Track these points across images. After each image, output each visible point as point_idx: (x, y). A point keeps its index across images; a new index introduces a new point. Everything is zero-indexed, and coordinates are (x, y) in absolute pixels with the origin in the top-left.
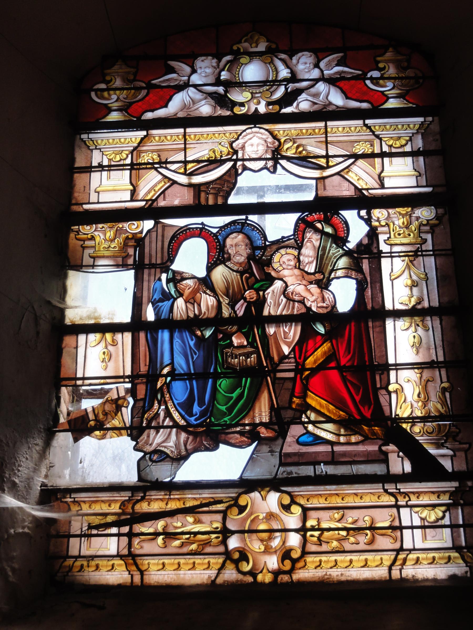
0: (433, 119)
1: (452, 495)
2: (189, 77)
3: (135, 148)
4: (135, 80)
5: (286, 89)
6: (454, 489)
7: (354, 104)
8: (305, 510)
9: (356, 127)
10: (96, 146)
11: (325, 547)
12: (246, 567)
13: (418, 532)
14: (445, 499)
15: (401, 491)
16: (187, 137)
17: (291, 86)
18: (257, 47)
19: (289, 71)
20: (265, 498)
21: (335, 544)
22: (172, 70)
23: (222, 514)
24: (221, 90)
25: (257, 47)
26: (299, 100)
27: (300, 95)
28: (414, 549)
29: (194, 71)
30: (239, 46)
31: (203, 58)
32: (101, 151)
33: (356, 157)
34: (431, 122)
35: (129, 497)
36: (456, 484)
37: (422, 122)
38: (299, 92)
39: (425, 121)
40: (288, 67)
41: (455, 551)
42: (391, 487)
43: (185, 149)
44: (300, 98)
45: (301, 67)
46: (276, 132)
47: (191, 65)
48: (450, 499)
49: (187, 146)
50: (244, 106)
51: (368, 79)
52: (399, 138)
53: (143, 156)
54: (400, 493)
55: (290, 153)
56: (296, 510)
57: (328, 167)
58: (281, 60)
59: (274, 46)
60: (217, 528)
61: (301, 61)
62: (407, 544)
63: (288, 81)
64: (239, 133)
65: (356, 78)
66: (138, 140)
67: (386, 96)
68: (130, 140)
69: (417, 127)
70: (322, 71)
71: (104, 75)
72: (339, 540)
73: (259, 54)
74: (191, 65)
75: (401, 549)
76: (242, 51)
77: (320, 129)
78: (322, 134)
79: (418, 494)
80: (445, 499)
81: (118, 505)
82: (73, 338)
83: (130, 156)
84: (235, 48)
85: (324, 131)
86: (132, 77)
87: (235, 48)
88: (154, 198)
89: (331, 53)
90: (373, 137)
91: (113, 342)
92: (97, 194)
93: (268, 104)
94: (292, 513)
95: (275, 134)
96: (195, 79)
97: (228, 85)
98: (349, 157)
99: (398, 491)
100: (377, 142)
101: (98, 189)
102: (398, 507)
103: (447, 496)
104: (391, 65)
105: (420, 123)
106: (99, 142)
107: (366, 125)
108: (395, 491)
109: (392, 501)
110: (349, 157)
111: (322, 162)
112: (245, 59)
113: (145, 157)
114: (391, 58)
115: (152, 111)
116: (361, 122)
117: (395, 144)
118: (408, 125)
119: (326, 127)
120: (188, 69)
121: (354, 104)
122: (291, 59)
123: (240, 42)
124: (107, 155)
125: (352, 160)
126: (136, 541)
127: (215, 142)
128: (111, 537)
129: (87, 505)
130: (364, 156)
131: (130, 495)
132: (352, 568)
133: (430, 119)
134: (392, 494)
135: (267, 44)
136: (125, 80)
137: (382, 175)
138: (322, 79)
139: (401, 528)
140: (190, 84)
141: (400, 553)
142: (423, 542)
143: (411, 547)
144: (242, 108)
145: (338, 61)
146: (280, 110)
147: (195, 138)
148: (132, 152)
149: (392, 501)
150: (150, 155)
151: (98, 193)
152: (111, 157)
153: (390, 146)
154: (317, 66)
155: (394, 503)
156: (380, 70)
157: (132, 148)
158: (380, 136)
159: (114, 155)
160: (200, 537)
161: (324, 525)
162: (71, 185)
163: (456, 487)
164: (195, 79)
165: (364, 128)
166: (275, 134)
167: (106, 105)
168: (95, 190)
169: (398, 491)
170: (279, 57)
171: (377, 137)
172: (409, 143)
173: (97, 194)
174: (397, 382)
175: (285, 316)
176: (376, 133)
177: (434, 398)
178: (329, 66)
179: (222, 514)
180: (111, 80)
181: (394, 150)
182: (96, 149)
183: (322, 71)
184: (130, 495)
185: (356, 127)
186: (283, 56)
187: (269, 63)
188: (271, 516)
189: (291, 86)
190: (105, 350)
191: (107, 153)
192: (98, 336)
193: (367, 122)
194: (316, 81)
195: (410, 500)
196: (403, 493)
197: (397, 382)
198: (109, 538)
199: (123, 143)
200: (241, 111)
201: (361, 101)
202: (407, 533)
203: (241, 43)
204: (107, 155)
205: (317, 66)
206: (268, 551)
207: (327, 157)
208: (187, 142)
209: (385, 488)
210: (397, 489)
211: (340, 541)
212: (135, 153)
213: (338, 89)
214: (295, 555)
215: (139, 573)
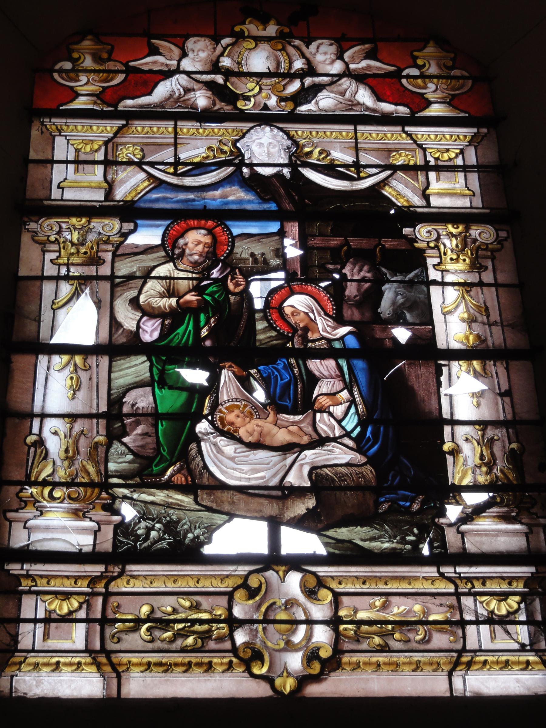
0: (488, 131)
1: (528, 581)
2: (179, 61)
3: (110, 140)
4: (109, 59)
5: (303, 84)
6: (530, 575)
7: (387, 107)
8: (337, 596)
9: (378, 134)
10: (60, 132)
11: (364, 646)
12: (259, 670)
13: (485, 629)
14: (520, 587)
15: (462, 575)
16: (178, 130)
17: (308, 81)
18: (265, 30)
19: (304, 60)
20: (284, 579)
21: (377, 640)
22: (155, 51)
23: (227, 597)
24: (220, 79)
25: (265, 29)
26: (319, 98)
27: (320, 91)
28: (481, 650)
29: (184, 55)
30: (243, 27)
31: (196, 39)
32: (66, 139)
33: (395, 168)
34: (486, 134)
35: (102, 573)
36: (533, 569)
37: (475, 133)
38: (317, 89)
39: (478, 132)
40: (303, 56)
41: (534, 653)
42: (448, 570)
43: (176, 145)
44: (321, 95)
45: (320, 58)
46: (294, 133)
47: (181, 46)
48: (524, 587)
49: (179, 141)
50: (250, 100)
51: (404, 77)
52: (448, 150)
53: (121, 149)
54: (460, 578)
55: (313, 160)
56: (326, 596)
57: (360, 178)
58: (295, 47)
59: (287, 30)
60: (220, 615)
61: (322, 49)
62: (472, 644)
63: (301, 75)
64: (245, 131)
65: (388, 75)
66: (115, 129)
67: (427, 99)
68: (456, 137)
69: (468, 139)
70: (347, 65)
71: (71, 51)
72: (381, 635)
73: (268, 39)
74: (181, 46)
75: (464, 650)
76: (246, 34)
77: (348, 133)
78: (351, 139)
79: (484, 580)
80: (520, 587)
81: (86, 582)
82: (30, 358)
83: (103, 148)
84: (237, 29)
85: (353, 134)
86: (105, 56)
87: (237, 29)
88: (136, 199)
89: (357, 43)
90: (415, 146)
91: (85, 366)
92: (61, 190)
93: (282, 99)
94: (319, 600)
95: (292, 135)
96: (187, 64)
97: (228, 73)
98: (385, 168)
99: (458, 575)
100: (419, 153)
101: (62, 185)
102: (458, 595)
103: (521, 585)
104: (433, 63)
105: (473, 134)
106: (419, 136)
107: (406, 133)
108: (453, 575)
109: (451, 589)
110: (385, 168)
111: (352, 173)
112: (248, 43)
113: (124, 150)
114: (434, 54)
115: (133, 98)
116: (399, 128)
117: (442, 157)
118: (458, 136)
119: (356, 130)
120: (176, 51)
121: (387, 107)
122: (308, 48)
123: (244, 23)
124: (73, 145)
125: (388, 172)
126: (109, 631)
127: (214, 139)
128: (77, 624)
129: (44, 581)
130: (405, 168)
131: (103, 570)
132: (402, 671)
133: (485, 130)
134: (450, 580)
135: (276, 27)
136: (97, 58)
137: (428, 191)
138: (347, 73)
139: (463, 623)
140: (181, 69)
141: (463, 654)
142: (491, 642)
143: (476, 647)
144: (247, 102)
145: (366, 53)
146: (295, 109)
147: (143, 131)
148: (106, 143)
149: (451, 589)
150: (131, 149)
151: (63, 188)
152: (80, 147)
153: (437, 159)
154: (340, 57)
155: (453, 591)
156: (419, 67)
157: (107, 139)
158: (424, 146)
159: (82, 145)
160: (197, 627)
161: (362, 615)
162: (24, 178)
163: (532, 573)
164: (187, 64)
165: (404, 135)
166: (292, 135)
167: (72, 88)
168: (59, 184)
169: (458, 575)
170: (292, 44)
171: (420, 146)
172: (461, 156)
173: (61, 190)
174: (453, 441)
175: (424, 621)
176: (418, 142)
177: (501, 463)
178: (353, 59)
179: (227, 597)
180: (80, 58)
181: (440, 163)
182: (60, 135)
183: (347, 65)
184: (103, 570)
185: (423, 135)
186: (297, 42)
187: (280, 50)
188: (290, 603)
189: (308, 81)
190: (74, 376)
191: (73, 142)
192: (65, 358)
193: (407, 129)
194: (340, 76)
195: (473, 587)
196: (465, 578)
197: (453, 441)
198: (74, 624)
199: (80, 132)
200: (246, 105)
201: (396, 104)
202: (471, 629)
203: (245, 24)
204: (73, 145)
205: (340, 57)
206: (290, 647)
207: (357, 165)
208: (178, 137)
209: (441, 571)
210: (455, 573)
211: (384, 638)
212: (110, 145)
213: (367, 88)
214: (325, 654)
215: (114, 675)
